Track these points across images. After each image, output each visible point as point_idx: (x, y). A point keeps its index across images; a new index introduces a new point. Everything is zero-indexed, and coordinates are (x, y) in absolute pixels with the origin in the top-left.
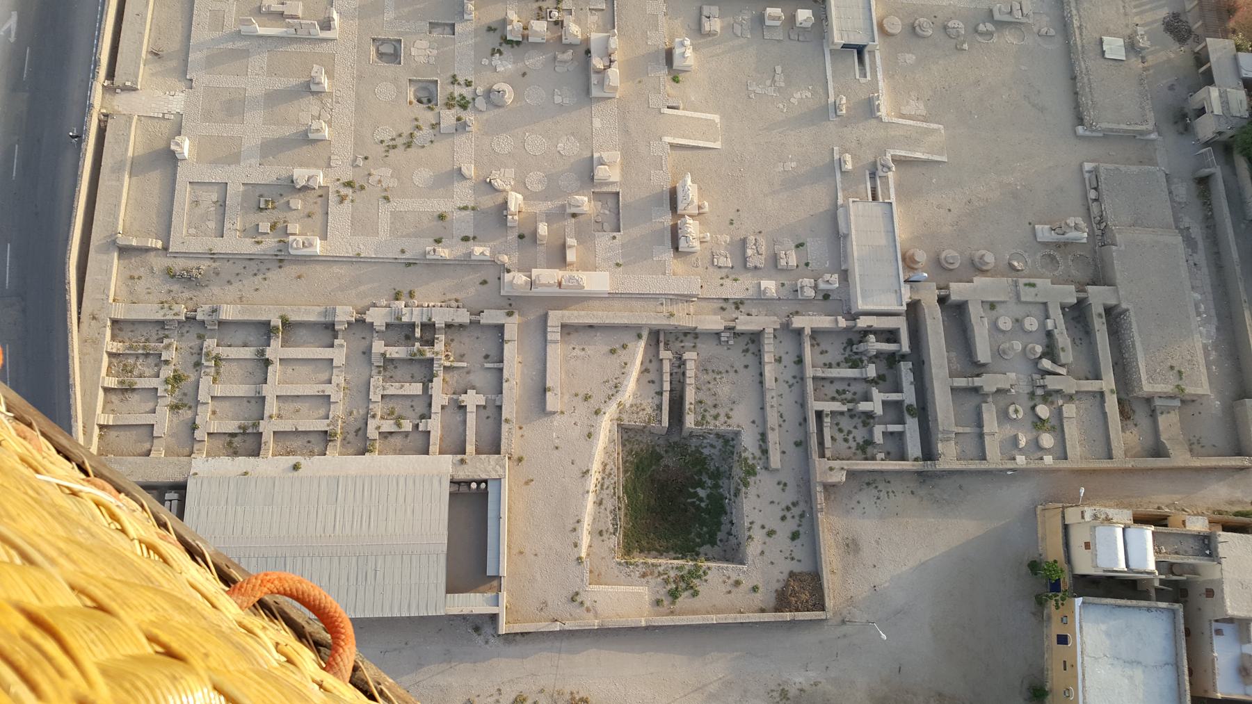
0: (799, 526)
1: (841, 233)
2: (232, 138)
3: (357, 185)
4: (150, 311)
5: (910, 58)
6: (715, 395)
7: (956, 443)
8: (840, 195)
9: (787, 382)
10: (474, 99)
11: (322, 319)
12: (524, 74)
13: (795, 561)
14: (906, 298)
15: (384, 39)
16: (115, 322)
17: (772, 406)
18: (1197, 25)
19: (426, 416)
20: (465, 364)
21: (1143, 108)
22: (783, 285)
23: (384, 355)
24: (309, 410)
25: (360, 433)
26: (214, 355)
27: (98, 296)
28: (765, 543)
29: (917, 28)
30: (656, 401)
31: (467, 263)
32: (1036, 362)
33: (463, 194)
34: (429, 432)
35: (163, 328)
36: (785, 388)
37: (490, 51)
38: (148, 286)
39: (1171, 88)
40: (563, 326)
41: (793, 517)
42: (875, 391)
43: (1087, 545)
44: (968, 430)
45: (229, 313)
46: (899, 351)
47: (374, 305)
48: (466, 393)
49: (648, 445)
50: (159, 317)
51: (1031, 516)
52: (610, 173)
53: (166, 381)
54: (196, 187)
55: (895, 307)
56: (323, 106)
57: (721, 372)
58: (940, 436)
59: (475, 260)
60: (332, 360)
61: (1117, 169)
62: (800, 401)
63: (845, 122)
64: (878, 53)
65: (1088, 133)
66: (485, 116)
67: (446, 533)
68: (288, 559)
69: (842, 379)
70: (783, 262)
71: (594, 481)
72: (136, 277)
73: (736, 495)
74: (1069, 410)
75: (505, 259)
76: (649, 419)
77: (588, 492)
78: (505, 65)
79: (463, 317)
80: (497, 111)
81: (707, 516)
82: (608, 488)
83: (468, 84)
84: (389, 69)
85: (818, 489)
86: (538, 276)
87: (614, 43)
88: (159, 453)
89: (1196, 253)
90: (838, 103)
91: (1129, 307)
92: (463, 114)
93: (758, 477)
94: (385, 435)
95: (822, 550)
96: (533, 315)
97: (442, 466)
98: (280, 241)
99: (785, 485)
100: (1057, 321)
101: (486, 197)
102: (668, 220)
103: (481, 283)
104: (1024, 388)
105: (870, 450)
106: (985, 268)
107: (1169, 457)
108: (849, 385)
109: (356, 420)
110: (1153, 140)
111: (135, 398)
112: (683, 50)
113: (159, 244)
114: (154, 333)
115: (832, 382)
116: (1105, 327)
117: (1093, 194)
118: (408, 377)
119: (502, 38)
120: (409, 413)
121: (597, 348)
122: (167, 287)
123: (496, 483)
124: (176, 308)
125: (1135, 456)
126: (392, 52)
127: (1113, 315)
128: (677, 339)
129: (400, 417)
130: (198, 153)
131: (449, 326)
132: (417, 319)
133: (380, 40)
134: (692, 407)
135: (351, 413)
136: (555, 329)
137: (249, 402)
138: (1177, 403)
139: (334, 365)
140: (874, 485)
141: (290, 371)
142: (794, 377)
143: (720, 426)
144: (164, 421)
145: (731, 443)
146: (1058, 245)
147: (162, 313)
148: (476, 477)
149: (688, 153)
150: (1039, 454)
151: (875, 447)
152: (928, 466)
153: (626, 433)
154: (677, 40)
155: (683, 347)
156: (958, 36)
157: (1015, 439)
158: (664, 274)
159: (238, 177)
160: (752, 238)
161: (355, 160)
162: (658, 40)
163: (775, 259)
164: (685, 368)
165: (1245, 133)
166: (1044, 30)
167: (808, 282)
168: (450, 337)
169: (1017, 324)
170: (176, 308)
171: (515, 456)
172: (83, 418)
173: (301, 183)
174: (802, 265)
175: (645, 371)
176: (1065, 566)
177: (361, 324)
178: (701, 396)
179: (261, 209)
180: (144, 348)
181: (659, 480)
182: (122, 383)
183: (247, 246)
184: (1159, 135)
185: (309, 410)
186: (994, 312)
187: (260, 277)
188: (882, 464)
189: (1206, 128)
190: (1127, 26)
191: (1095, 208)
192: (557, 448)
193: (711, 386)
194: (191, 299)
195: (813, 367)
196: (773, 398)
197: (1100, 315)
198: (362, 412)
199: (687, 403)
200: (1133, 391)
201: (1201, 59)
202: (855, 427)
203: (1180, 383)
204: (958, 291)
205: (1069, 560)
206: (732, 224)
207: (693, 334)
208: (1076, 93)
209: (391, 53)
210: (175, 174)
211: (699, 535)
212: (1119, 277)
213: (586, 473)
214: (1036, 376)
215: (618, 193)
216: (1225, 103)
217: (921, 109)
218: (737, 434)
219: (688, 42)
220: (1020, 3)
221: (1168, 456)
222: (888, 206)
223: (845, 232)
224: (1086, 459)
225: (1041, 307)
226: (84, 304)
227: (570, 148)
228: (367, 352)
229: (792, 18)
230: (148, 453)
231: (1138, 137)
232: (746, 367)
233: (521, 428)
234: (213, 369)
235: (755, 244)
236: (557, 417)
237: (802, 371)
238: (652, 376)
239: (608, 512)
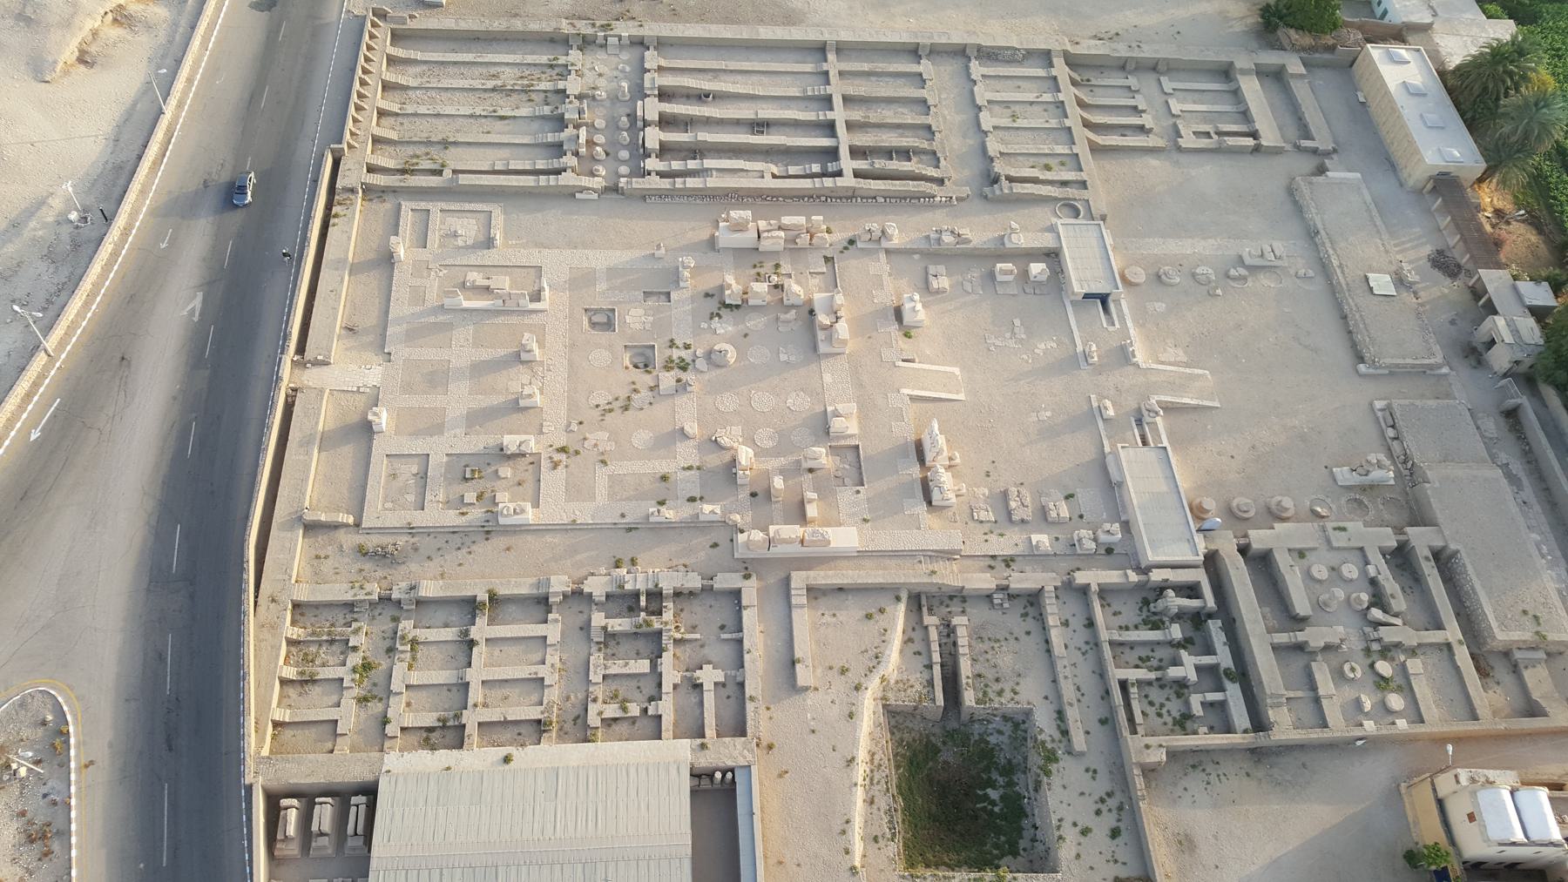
0: (1119, 820)
1: (1114, 481)
2: (435, 409)
3: (571, 450)
4: (338, 592)
5: (1161, 307)
6: (995, 666)
7: (1289, 710)
8: (1106, 442)
9: (1079, 649)
10: (694, 361)
11: (535, 591)
12: (746, 335)
13: (1119, 864)
14: (1202, 546)
15: (597, 310)
16: (297, 606)
17: (1066, 677)
18: (1464, 260)
19: (656, 697)
20: (698, 636)
21: (1426, 341)
22: (1057, 539)
23: (605, 628)
24: (519, 696)
25: (579, 721)
26: (410, 638)
27: (280, 577)
28: (1079, 844)
29: (1163, 277)
30: (926, 676)
31: (695, 525)
32: (1364, 613)
33: (687, 454)
34: (660, 716)
35: (352, 612)
36: (1078, 657)
37: (709, 316)
38: (337, 566)
39: (1453, 322)
40: (810, 589)
41: (1110, 810)
42: (1183, 653)
43: (1471, 817)
44: (1299, 694)
45: (429, 589)
46: (1204, 608)
47: (593, 574)
48: (701, 668)
49: (921, 734)
50: (349, 597)
51: (1394, 796)
52: (848, 425)
53: (354, 670)
54: (392, 459)
55: (1189, 557)
56: (534, 375)
57: (999, 641)
58: (1269, 701)
59: (704, 522)
60: (546, 637)
61: (1413, 404)
62: (1098, 671)
63: (1099, 370)
64: (1124, 303)
65: (1371, 371)
66: (707, 377)
67: (689, 831)
68: (500, 868)
69: (1144, 644)
70: (1053, 514)
71: (861, 772)
72: (323, 556)
73: (1036, 790)
74: (1415, 665)
75: (737, 518)
76: (920, 697)
77: (856, 785)
78: (725, 327)
79: (694, 582)
80: (718, 371)
81: (1003, 823)
82: (878, 782)
83: (687, 347)
84: (603, 337)
85: (1136, 771)
86: (777, 532)
87: (839, 299)
88: (343, 745)
89: (1523, 490)
90: (1087, 350)
91: (1459, 548)
92: (684, 376)
93: (1061, 763)
94: (609, 722)
95: (1150, 846)
96: (773, 579)
97: (678, 753)
98: (488, 511)
99: (1095, 771)
100: (1379, 568)
101: (714, 455)
102: (916, 471)
103: (711, 547)
104: (1355, 644)
105: (1189, 724)
106: (1285, 515)
107: (1547, 716)
108: (1153, 651)
109: (573, 706)
110: (1445, 375)
111: (316, 690)
112: (913, 304)
113: (351, 520)
114: (341, 616)
115: (1132, 648)
116: (1435, 571)
117: (1391, 433)
118: (633, 654)
119: (720, 303)
120: (637, 695)
121: (851, 612)
122: (358, 566)
123: (745, 771)
124: (368, 587)
125: (1508, 716)
126: (605, 320)
127: (1441, 558)
128: (942, 603)
129: (625, 700)
130: (396, 425)
131: (677, 594)
132: (641, 586)
133: (592, 310)
134: (970, 681)
135: (568, 698)
136: (799, 592)
137: (449, 690)
138: (1542, 655)
139: (548, 642)
140: (1201, 768)
141: (497, 652)
142: (1087, 643)
143: (1005, 703)
144: (349, 715)
145: (1022, 727)
146: (1364, 489)
147: (352, 592)
148: (721, 765)
149: (930, 405)
150: (1390, 719)
151: (1194, 722)
152: (1261, 739)
153: (894, 716)
154: (905, 296)
155: (950, 612)
156: (1210, 282)
157: (1358, 703)
158: (919, 528)
159: (439, 450)
160: (1013, 490)
161: (569, 424)
162: (885, 297)
163: (1043, 512)
164: (956, 637)
165: (1544, 358)
166: (1301, 273)
167: (1085, 533)
168: (679, 607)
169: (1334, 573)
170: (368, 587)
171: (764, 743)
172: (256, 712)
173: (513, 449)
174: (1075, 517)
175: (908, 641)
176: (1450, 849)
177: (578, 596)
178: (979, 668)
179: (466, 480)
180: (329, 634)
181: (939, 781)
182: (302, 673)
183: (451, 518)
184: (1451, 369)
185: (519, 696)
186: (1304, 561)
187: (464, 551)
188: (1207, 739)
189: (1500, 359)
190: (1391, 262)
191: (1395, 445)
192: (813, 731)
193: (989, 656)
194: (386, 578)
195: (1107, 629)
196: (1065, 667)
197: (1427, 559)
198: (581, 696)
199: (963, 677)
200: (1485, 643)
201: (1477, 292)
202: (1168, 699)
203: (1539, 629)
204: (1259, 539)
205: (1452, 841)
206: (988, 476)
207: (959, 597)
208: (1350, 332)
209: (605, 322)
210: (370, 448)
211: (996, 846)
212: (1440, 517)
213: (851, 761)
214: (1368, 629)
215: (857, 447)
216: (1515, 332)
217: (1183, 358)
218: (1028, 713)
219: (917, 297)
220: (1271, 246)
221: (1545, 714)
222: (1096, 227)
223: (1120, 480)
224: (1446, 721)
225: (1358, 552)
226: (262, 586)
227: (800, 403)
228: (586, 628)
229: (1025, 274)
230: (332, 751)
231: (1428, 372)
232: (1028, 633)
233: (768, 709)
234: (409, 655)
235: (1018, 496)
236: (810, 694)
237: (1095, 635)
238: (918, 646)
239: (882, 813)
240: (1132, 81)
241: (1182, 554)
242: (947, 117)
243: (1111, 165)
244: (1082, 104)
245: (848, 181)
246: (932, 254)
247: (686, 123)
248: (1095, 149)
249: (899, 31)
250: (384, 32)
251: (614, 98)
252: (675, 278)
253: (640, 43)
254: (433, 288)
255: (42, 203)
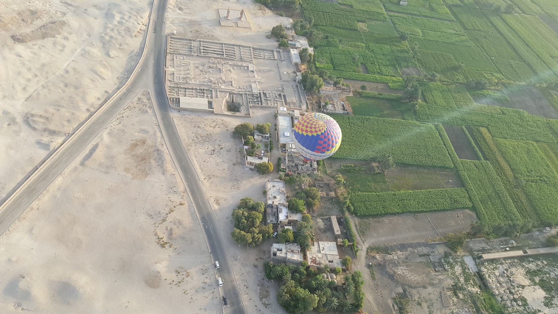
31: (207, 85)
33: (206, 79)
64: (255, 73)
121: (223, 93)
127: (284, 96)
159: (181, 77)
204: (265, 92)
207: (234, 94)
218: (240, 103)
227: (219, 77)
240: (261, 51)
241: (257, 92)
242: (237, 52)
243: (256, 59)
244: (253, 53)
245: (225, 57)
246: (234, 65)
247: (227, 52)
248: (254, 58)
249: (232, 43)
250: (169, 37)
251: (197, 47)
252: (205, 64)
253: (200, 41)
254: (178, 63)
255: (134, 50)
